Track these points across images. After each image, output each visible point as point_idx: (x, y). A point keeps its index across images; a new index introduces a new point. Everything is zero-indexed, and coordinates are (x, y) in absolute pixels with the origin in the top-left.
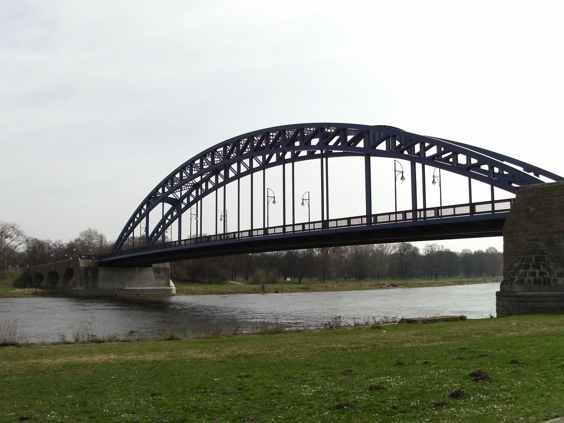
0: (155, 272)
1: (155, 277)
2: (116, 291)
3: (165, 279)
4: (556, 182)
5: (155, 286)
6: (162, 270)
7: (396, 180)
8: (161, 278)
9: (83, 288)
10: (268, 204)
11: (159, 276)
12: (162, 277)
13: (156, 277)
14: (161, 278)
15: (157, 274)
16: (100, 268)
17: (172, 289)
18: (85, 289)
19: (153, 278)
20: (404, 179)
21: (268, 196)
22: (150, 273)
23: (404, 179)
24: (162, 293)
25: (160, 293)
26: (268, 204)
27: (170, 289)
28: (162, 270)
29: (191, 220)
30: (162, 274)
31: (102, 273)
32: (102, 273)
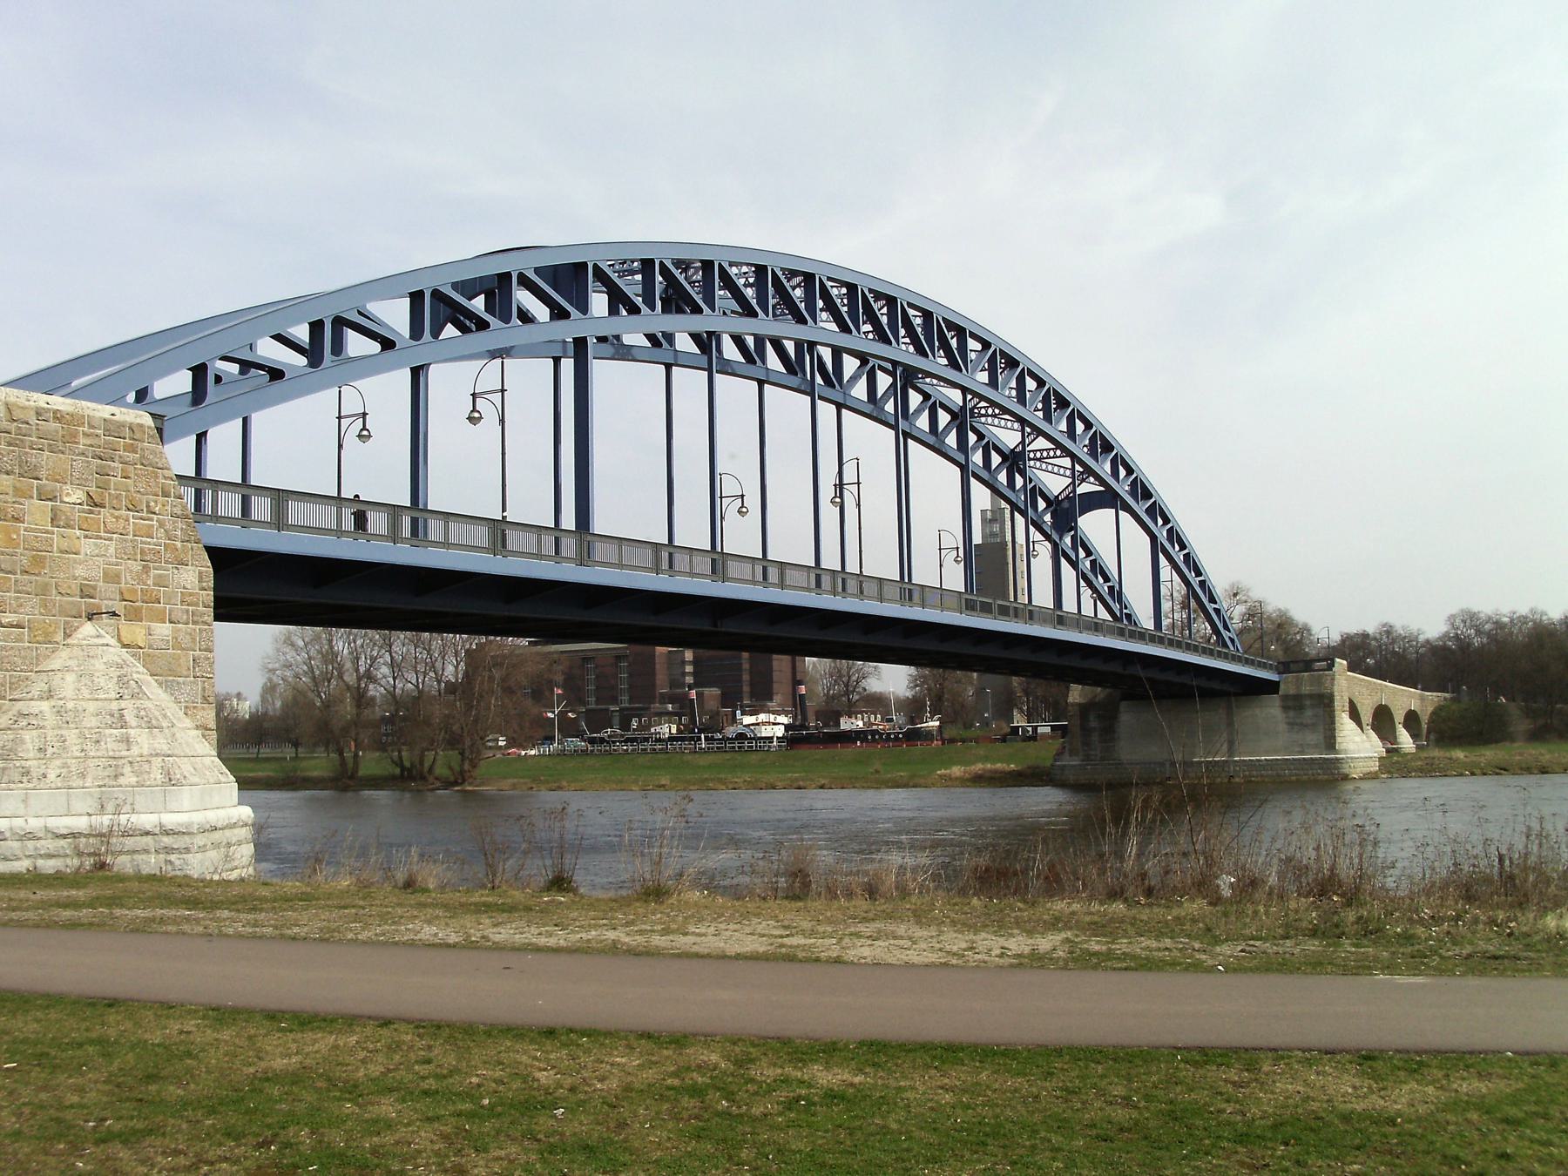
0: (1285, 708)
1: (1289, 724)
2: (1168, 765)
3: (1321, 728)
4: (793, 357)
5: (1288, 751)
6: (1308, 703)
7: (340, 446)
8: (1306, 726)
9: (1075, 762)
10: (722, 518)
11: (1298, 721)
12: (1309, 722)
13: (1291, 724)
14: (1306, 726)
15: (1292, 714)
16: (1123, 705)
17: (1343, 759)
18: (1080, 765)
19: (1282, 727)
20: (370, 436)
21: (721, 498)
22: (1272, 711)
23: (370, 436)
24: (1310, 772)
25: (1302, 772)
26: (722, 518)
27: (1337, 759)
28: (1308, 703)
29: (941, 565)
30: (1309, 713)
31: (1127, 717)
32: (1127, 717)
